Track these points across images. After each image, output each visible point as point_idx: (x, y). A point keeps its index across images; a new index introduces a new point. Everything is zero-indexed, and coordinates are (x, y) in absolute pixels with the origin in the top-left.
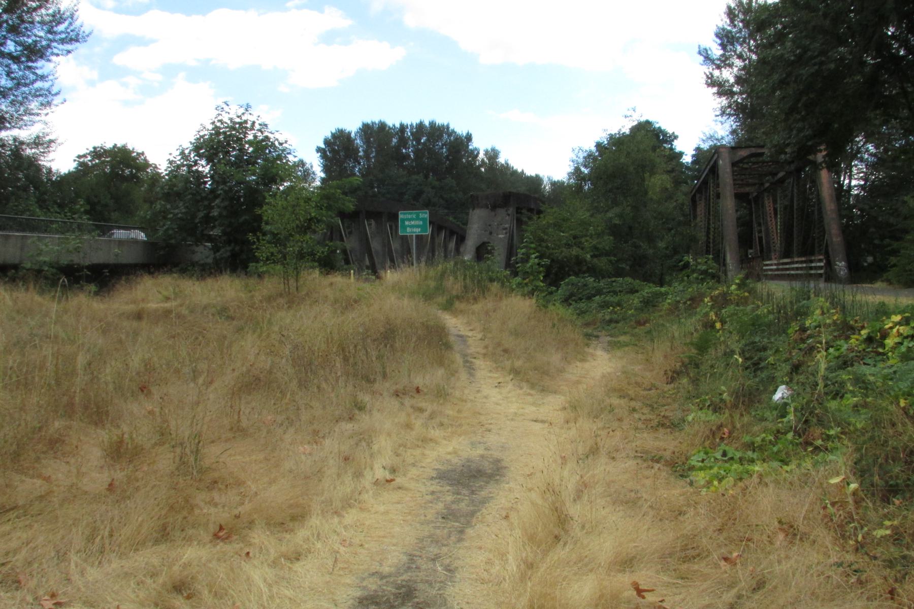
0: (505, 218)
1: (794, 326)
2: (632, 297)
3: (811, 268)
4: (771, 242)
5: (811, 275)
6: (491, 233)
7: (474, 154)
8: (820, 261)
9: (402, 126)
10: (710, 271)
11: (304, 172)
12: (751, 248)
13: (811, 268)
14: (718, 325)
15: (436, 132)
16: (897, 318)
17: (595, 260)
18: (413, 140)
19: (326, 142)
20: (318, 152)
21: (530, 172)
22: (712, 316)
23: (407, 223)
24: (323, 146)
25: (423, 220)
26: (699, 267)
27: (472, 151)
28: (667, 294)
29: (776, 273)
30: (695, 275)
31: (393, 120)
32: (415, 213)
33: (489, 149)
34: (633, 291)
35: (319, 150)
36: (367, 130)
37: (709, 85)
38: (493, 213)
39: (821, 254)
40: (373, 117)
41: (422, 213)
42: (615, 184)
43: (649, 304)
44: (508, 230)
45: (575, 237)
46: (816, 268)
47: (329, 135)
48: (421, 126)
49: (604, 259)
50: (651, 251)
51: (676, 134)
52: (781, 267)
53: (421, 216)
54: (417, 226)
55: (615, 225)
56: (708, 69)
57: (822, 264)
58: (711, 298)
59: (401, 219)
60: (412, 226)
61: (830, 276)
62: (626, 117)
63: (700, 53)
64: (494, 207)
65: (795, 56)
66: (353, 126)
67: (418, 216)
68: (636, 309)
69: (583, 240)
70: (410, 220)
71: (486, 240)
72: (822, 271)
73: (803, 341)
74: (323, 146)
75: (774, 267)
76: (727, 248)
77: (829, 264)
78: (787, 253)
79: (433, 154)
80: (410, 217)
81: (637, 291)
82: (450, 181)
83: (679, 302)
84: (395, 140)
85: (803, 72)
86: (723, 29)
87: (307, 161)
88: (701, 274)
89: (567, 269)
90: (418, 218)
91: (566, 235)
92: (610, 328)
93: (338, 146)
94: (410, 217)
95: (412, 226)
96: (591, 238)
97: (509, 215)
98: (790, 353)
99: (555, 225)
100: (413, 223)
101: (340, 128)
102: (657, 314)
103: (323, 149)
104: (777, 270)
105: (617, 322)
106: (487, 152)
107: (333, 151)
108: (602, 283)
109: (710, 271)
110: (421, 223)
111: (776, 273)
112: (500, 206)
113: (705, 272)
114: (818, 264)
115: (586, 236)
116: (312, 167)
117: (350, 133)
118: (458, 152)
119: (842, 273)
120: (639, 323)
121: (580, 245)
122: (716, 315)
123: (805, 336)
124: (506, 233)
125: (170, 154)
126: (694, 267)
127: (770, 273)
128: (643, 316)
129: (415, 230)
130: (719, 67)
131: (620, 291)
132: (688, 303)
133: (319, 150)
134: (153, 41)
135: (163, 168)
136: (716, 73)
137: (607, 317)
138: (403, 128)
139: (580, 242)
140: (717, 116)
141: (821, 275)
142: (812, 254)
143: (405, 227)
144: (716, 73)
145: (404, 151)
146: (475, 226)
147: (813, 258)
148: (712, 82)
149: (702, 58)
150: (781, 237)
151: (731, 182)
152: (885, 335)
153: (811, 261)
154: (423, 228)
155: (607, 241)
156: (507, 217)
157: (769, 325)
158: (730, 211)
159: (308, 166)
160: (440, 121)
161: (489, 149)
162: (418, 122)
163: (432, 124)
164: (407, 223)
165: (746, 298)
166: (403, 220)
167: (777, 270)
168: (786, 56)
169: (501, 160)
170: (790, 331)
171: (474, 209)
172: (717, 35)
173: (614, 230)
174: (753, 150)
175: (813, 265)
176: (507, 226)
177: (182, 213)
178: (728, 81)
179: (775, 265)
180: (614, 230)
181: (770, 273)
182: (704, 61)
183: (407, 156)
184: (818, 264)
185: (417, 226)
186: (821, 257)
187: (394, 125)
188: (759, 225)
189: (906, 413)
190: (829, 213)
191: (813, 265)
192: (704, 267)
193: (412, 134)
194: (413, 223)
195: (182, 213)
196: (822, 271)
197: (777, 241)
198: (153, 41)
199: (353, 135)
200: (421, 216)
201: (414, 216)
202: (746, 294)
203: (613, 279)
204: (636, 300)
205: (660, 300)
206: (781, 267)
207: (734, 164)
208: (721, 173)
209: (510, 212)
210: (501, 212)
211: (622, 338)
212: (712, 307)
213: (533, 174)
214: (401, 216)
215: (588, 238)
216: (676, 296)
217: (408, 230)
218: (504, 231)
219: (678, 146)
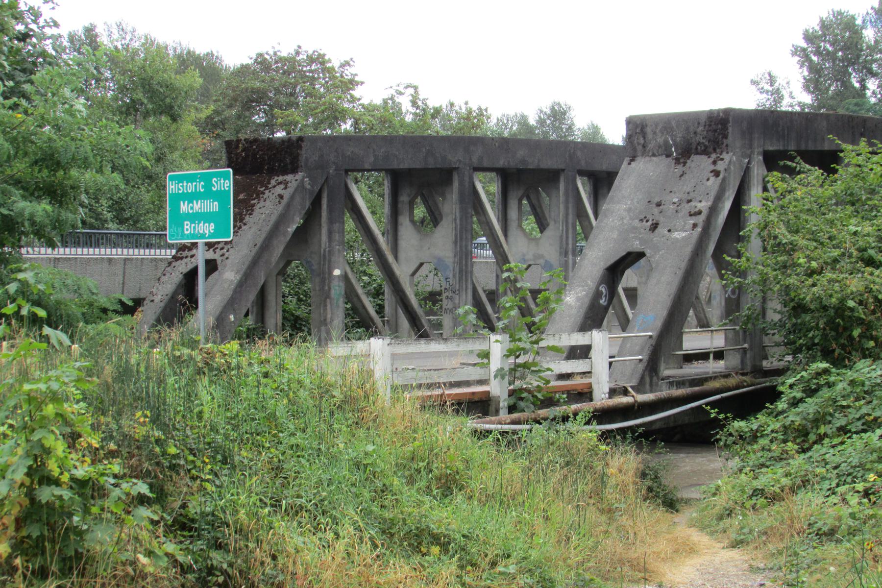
6: (655, 227)
19: (809, 37)
25: (219, 196)
35: (797, 51)
38: (679, 169)
54: (204, 217)
60: (195, 218)
67: (208, 185)
80: (190, 187)
89: (856, 333)
90: (208, 194)
94: (190, 187)
95: (195, 218)
98: (269, 448)
100: (197, 206)
101: (836, 9)
103: (804, 50)
110: (214, 206)
112: (705, 152)
117: (853, 18)
124: (695, 226)
133: (797, 51)
135: (621, 144)
143: (180, 219)
156: (712, 179)
164: (184, 207)
185: (204, 217)
194: (197, 206)
198: (362, 83)
199: (859, 22)
201: (200, 187)
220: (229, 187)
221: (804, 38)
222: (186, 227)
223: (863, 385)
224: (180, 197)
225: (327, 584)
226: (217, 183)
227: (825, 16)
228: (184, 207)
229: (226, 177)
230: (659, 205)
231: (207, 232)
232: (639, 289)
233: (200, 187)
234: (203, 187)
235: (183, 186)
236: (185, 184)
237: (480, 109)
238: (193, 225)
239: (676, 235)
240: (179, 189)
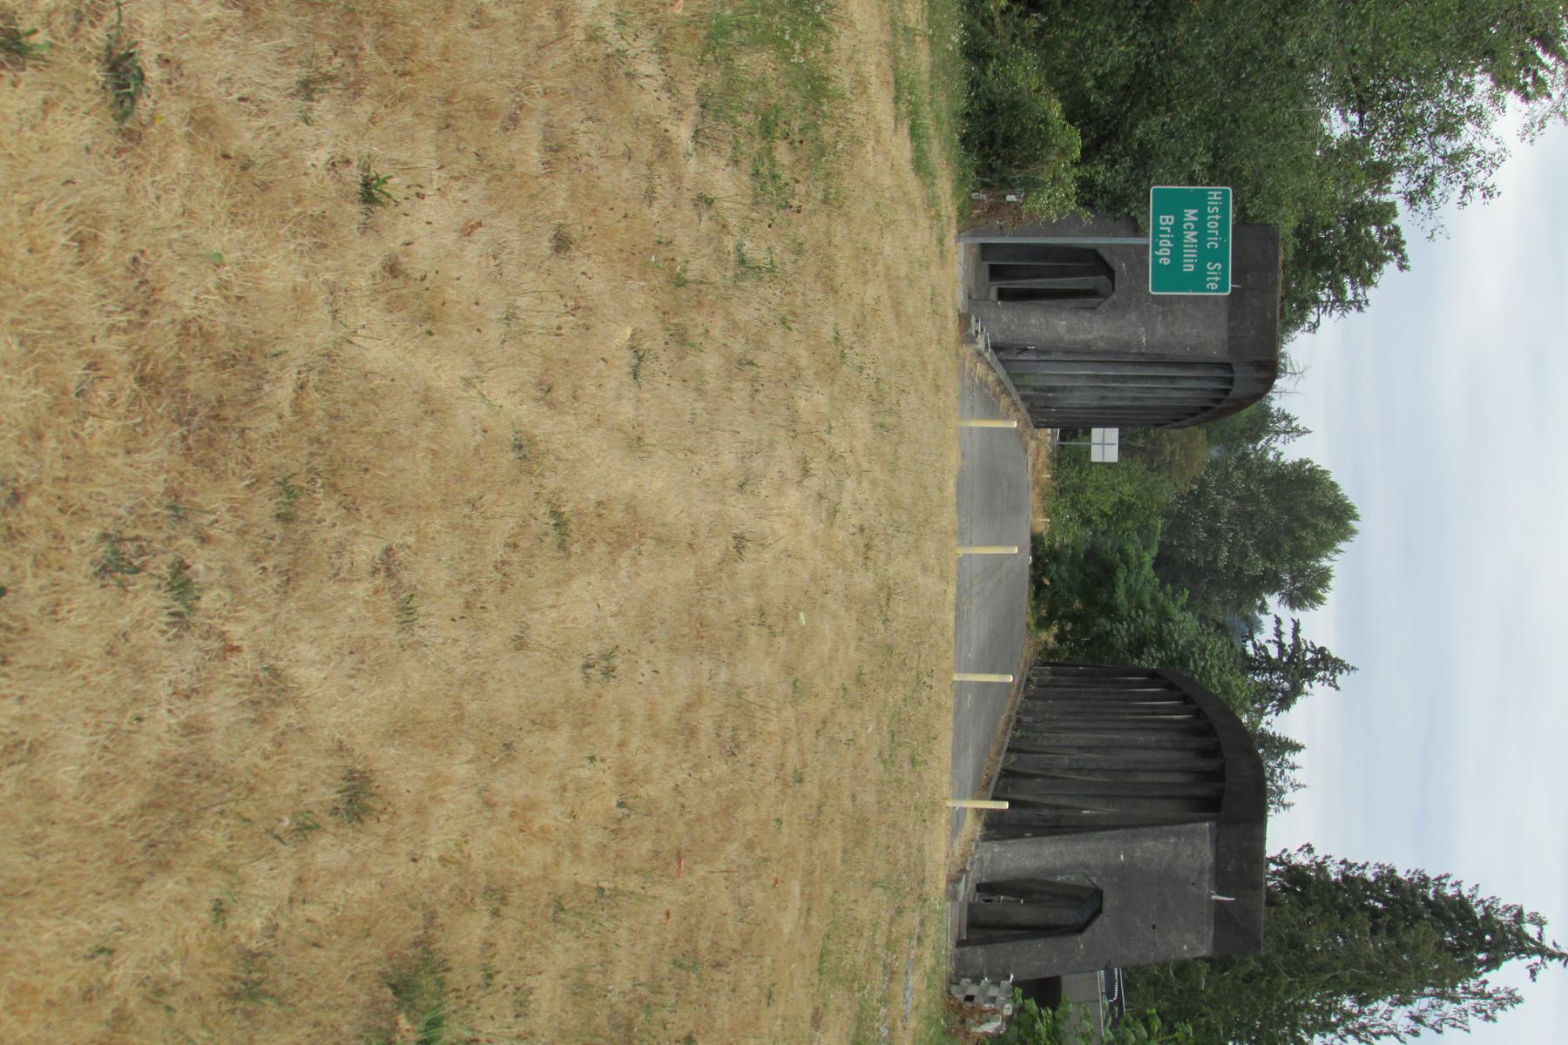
25: (1198, 279)
27: (1379, 878)
32: (1223, 245)
53: (1213, 268)
54: (1177, 253)
62: (1431, 237)
70: (1201, 226)
80: (1212, 226)
90: (1204, 255)
94: (1212, 226)
95: (1177, 230)
100: (1190, 236)
125: (1499, 193)
129: (1166, 243)
134: (1534, 980)
164: (1190, 215)
185: (1177, 253)
189: (822, 955)
194: (1190, 236)
198: (1534, 980)
214: (1215, 193)
217: (1167, 220)
220: (1210, 290)
221: (1288, 708)
222: (1167, 217)
223: (884, 1001)
224: (1200, 203)
226: (1216, 270)
228: (1190, 215)
229: (1222, 287)
231: (1160, 253)
232: (1065, 979)
233: (1212, 243)
234: (1212, 246)
235: (1214, 214)
236: (1217, 217)
237: (1353, 532)
238: (1169, 229)
240: (1212, 206)
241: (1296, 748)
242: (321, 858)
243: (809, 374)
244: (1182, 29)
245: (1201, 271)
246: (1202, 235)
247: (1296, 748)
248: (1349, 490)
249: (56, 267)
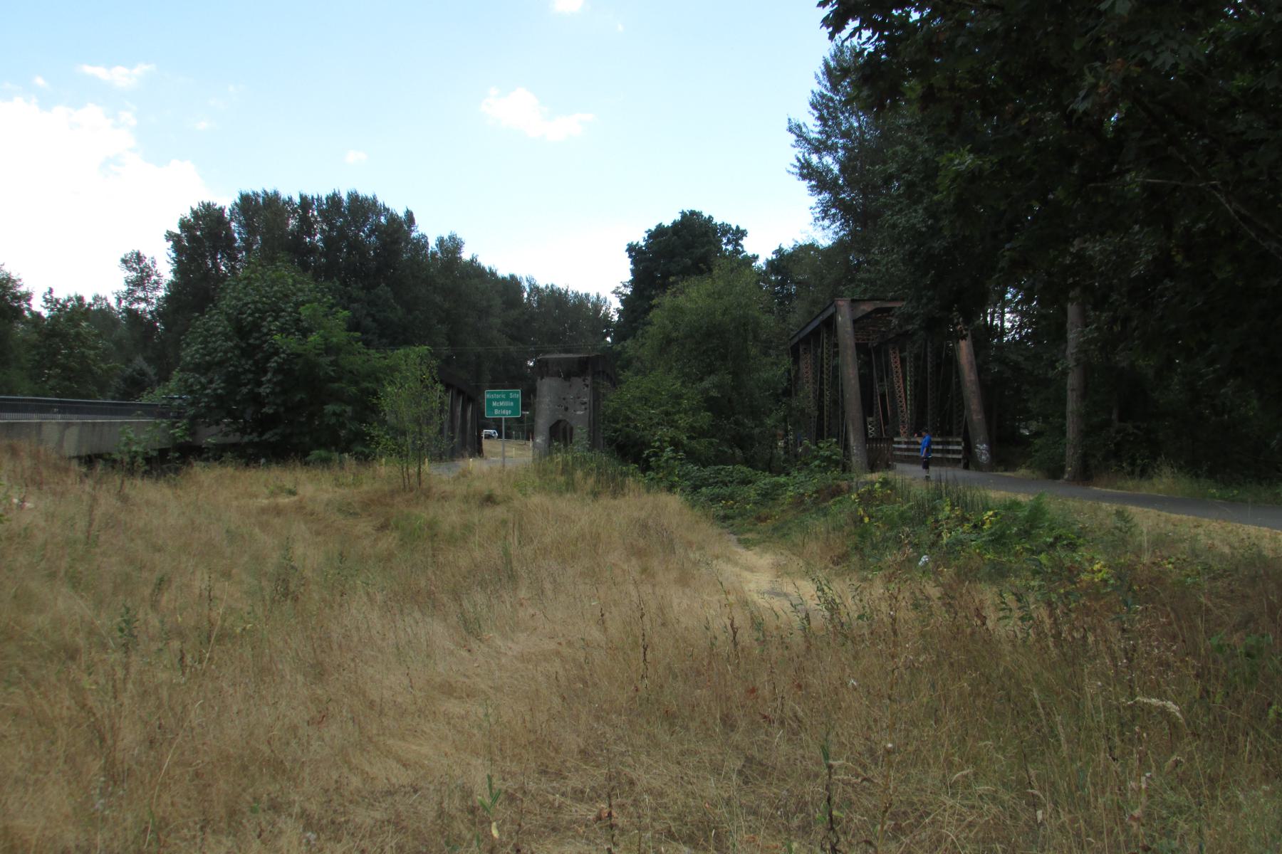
0: (581, 389)
1: (931, 520)
2: (746, 489)
3: (948, 451)
4: (899, 411)
5: (948, 459)
6: (566, 409)
7: (421, 244)
8: (958, 443)
9: (303, 198)
10: (834, 457)
11: (142, 271)
12: (871, 415)
13: (948, 451)
14: (866, 520)
15: (361, 208)
16: (990, 513)
17: (694, 443)
18: (323, 222)
19: (184, 225)
20: (168, 240)
21: (503, 272)
22: (861, 511)
23: (494, 404)
24: (178, 231)
25: (514, 400)
26: (822, 453)
28: (785, 485)
29: (906, 453)
30: (817, 462)
31: (290, 190)
32: (504, 393)
33: (446, 237)
34: (745, 482)
35: (170, 236)
36: (246, 203)
37: (803, 177)
38: (567, 384)
39: (958, 435)
40: (259, 185)
41: (513, 392)
42: (711, 345)
43: (768, 496)
44: (587, 406)
45: (667, 414)
46: (954, 452)
47: (188, 215)
48: (334, 200)
49: (704, 441)
50: (757, 431)
51: (742, 228)
52: (912, 447)
53: (512, 396)
54: (507, 408)
55: (713, 398)
56: (799, 152)
57: (960, 448)
58: (858, 495)
59: (488, 399)
60: (500, 408)
61: (969, 460)
63: (790, 130)
64: (568, 376)
65: (927, 226)
66: (226, 200)
68: (755, 503)
69: (676, 417)
70: (498, 400)
71: (561, 417)
72: (960, 456)
73: (937, 528)
74: (178, 231)
75: (904, 446)
76: (851, 428)
77: (969, 450)
78: (917, 429)
79: (356, 245)
80: (498, 396)
81: (750, 482)
82: (383, 290)
83: (803, 494)
84: (292, 222)
85: (936, 245)
86: (822, 96)
87: (147, 253)
88: (822, 462)
90: (508, 399)
91: (657, 411)
92: (725, 525)
93: (201, 230)
94: (498, 396)
95: (500, 408)
96: (685, 414)
97: (587, 386)
99: (640, 399)
100: (501, 404)
101: (206, 202)
102: (778, 509)
104: (908, 450)
105: (733, 518)
106: (441, 242)
107: (192, 238)
108: (707, 472)
109: (834, 457)
110: (512, 404)
111: (906, 453)
112: (578, 375)
113: (828, 459)
114: (956, 447)
115: (679, 412)
116: (154, 262)
117: (222, 210)
118: (396, 242)
119: (983, 457)
120: (759, 519)
121: (673, 424)
122: (864, 510)
123: (937, 526)
124: (586, 409)
126: (816, 453)
127: (898, 453)
128: (764, 511)
129: (504, 412)
130: (817, 150)
131: (732, 482)
132: (814, 495)
133: (170, 236)
136: (814, 159)
137: (722, 513)
138: (306, 203)
139: (673, 421)
140: (817, 219)
141: (959, 460)
142: (950, 433)
143: (492, 409)
144: (814, 159)
145: (308, 239)
146: (547, 400)
147: (950, 440)
148: (807, 171)
149: (794, 137)
150: (911, 405)
151: (853, 344)
152: (983, 523)
153: (949, 443)
154: (514, 409)
155: (705, 418)
156: (586, 389)
157: (912, 519)
158: (853, 382)
159: (149, 262)
160: (365, 191)
161: (446, 237)
162: (330, 193)
163: (354, 198)
164: (494, 404)
165: (889, 496)
166: (490, 401)
167: (908, 450)
168: (918, 226)
169: (466, 255)
170: (928, 523)
171: (542, 378)
172: (814, 106)
173: (711, 404)
174: (878, 304)
175: (950, 447)
176: (585, 400)
177: (221, 388)
178: (831, 170)
179: (906, 443)
180: (711, 404)
181: (898, 453)
182: (797, 141)
183: (312, 249)
184: (956, 447)
185: (507, 408)
186: (959, 439)
187: (290, 199)
188: (881, 380)
190: (968, 384)
191: (950, 447)
192: (828, 453)
193: (321, 212)
195: (221, 388)
196: (960, 456)
197: (906, 411)
199: (227, 214)
200: (512, 396)
201: (504, 396)
202: (889, 492)
203: (721, 467)
204: (752, 492)
205: (780, 492)
206: (912, 447)
207: (855, 322)
208: (840, 331)
209: (588, 382)
210: (577, 381)
211: (749, 536)
212: (860, 504)
213: (507, 275)
215: (682, 415)
216: (798, 488)
217: (496, 412)
218: (583, 407)
219: (749, 246)
224: (490, 401)
225: (33, 850)
227: (196, 207)
229: (518, 393)
230: (564, 399)
233: (504, 396)
239: (578, 413)
241: (192, 209)
242: (837, 801)
243: (58, 461)
244: (331, 545)
245: (513, 400)
246: (501, 400)
247: (192, 209)
248: (658, 224)
249: (1108, 644)
